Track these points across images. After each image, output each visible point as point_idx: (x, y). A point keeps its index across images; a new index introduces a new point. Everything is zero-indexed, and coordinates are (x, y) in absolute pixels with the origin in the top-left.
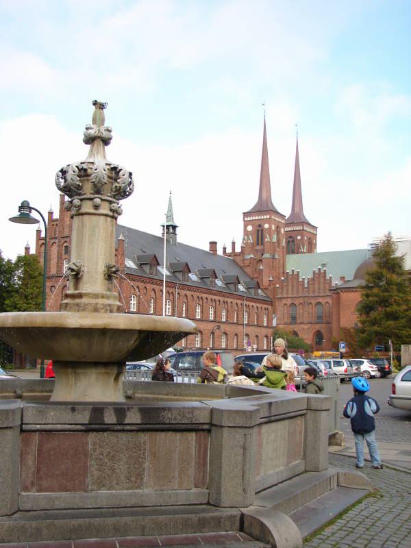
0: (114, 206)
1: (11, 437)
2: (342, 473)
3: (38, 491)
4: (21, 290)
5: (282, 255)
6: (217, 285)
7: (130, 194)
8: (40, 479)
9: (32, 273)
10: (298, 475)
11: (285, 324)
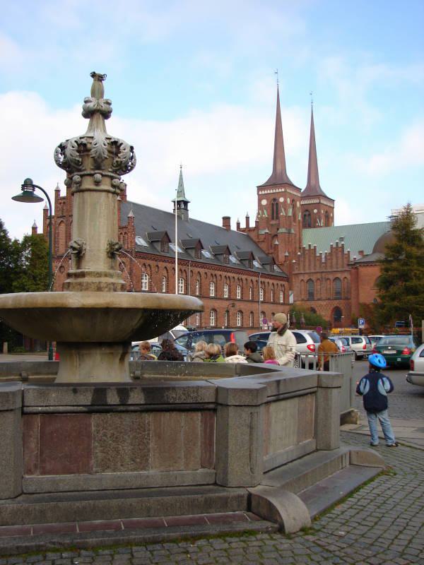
0: (116, 181)
1: (11, 423)
2: (354, 451)
3: (42, 474)
4: (29, 271)
5: (298, 229)
6: (231, 262)
7: (132, 168)
8: (43, 461)
9: (39, 253)
10: (308, 454)
11: (303, 300)
